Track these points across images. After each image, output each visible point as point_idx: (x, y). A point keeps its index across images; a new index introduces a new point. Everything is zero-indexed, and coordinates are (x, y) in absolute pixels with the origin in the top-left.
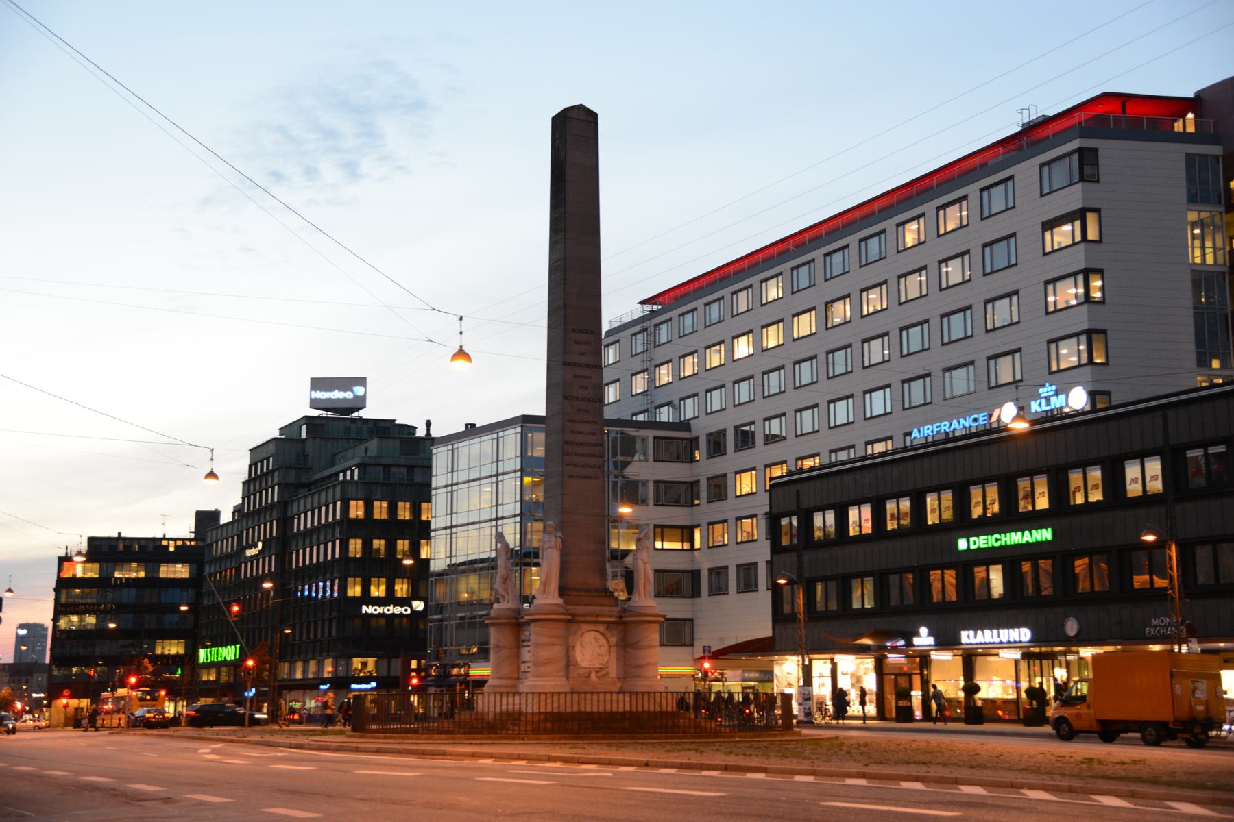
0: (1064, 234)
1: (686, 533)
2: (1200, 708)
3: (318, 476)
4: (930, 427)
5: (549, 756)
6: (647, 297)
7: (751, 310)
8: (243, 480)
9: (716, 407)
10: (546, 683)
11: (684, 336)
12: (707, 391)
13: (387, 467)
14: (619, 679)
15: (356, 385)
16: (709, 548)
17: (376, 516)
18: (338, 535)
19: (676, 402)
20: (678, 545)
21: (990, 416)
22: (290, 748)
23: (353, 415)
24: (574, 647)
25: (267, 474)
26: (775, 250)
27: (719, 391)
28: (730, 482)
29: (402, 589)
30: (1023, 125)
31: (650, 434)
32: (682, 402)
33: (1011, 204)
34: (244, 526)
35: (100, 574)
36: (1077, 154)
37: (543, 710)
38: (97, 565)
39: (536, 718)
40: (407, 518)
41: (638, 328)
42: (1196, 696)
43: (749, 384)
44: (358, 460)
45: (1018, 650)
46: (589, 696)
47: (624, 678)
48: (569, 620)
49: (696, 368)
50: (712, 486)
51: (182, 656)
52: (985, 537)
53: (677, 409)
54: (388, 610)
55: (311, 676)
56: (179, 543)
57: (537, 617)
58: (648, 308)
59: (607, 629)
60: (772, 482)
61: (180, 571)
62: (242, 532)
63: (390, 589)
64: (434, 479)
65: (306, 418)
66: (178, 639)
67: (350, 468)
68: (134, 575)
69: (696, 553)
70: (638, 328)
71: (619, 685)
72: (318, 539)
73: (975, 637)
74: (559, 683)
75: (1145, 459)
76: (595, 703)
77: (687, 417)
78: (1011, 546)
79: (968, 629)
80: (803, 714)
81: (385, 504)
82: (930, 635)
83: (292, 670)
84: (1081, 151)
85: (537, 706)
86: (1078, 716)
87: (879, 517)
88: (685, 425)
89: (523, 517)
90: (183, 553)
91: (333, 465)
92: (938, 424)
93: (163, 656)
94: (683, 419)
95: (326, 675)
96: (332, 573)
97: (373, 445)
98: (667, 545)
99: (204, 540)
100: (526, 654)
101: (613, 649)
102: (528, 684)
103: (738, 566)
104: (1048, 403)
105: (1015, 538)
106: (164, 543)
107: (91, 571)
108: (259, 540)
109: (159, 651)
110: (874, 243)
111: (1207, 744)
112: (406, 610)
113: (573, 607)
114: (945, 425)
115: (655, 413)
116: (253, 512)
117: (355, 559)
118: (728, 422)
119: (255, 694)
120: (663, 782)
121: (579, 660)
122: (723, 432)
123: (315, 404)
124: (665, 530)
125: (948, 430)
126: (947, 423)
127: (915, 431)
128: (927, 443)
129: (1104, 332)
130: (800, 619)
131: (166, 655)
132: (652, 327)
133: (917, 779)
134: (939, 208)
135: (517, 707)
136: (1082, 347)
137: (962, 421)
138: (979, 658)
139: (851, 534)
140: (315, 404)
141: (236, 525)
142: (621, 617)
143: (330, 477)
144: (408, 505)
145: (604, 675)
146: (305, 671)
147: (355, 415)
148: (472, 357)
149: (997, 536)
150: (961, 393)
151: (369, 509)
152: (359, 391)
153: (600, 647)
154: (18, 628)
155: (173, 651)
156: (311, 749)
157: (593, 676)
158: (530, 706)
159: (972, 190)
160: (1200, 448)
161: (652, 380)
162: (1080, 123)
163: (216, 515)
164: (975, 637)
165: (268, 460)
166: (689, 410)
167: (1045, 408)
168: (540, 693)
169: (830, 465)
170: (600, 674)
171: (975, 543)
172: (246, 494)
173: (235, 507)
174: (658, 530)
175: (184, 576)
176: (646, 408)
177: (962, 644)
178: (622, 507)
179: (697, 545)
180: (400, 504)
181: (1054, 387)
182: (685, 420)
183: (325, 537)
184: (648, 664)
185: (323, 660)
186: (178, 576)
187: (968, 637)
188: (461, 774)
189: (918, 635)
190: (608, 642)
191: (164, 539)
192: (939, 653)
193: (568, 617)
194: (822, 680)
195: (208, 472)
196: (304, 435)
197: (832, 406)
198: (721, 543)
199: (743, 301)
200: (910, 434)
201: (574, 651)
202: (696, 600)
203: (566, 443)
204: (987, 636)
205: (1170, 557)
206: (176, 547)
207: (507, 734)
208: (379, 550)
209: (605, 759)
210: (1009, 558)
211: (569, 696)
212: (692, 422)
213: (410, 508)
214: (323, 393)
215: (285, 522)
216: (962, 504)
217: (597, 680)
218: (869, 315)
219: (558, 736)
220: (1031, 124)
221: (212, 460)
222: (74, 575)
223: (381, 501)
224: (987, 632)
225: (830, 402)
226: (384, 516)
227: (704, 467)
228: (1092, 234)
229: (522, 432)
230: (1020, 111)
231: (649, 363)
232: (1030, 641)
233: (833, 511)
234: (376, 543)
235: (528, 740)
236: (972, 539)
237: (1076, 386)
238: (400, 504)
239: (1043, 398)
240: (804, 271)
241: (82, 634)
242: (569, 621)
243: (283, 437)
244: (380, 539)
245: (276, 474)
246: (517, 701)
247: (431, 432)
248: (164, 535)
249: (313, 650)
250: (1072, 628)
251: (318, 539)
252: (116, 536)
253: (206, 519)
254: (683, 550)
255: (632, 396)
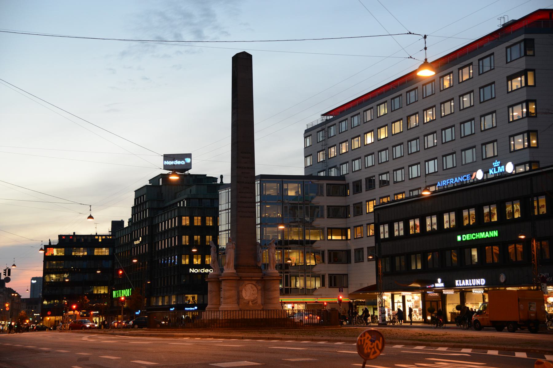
0: (516, 83)
1: (344, 232)
2: (533, 315)
3: (168, 204)
4: (445, 181)
5: (210, 336)
6: (324, 113)
7: (347, 130)
8: (132, 206)
9: (370, 164)
10: (228, 307)
11: (395, 110)
12: (393, 147)
13: (200, 200)
14: (262, 304)
15: (187, 157)
16: (355, 239)
17: (196, 224)
18: (177, 234)
19: (338, 166)
20: (339, 238)
21: (471, 176)
22: (120, 335)
23: (186, 172)
24: (242, 291)
25: (143, 203)
26: (384, 89)
27: (400, 146)
28: (364, 207)
29: (209, 260)
30: (503, 25)
31: (325, 183)
32: (341, 166)
33: (417, 100)
34: (133, 229)
35: (65, 253)
36: (523, 42)
37: (226, 318)
38: (63, 249)
39: (224, 321)
40: (211, 225)
41: (320, 129)
42: (531, 309)
43: (372, 156)
44: (186, 196)
45: (482, 289)
46: (246, 312)
47: (265, 304)
48: (239, 279)
49: (336, 154)
50: (356, 207)
51: (106, 294)
52: (469, 235)
53: (339, 169)
54: (202, 271)
55: (166, 304)
56: (104, 237)
57: (226, 278)
58: (325, 118)
59: (257, 283)
60: (375, 208)
61: (105, 252)
62: (132, 232)
63: (203, 260)
64: (220, 206)
65: (161, 174)
66: (104, 286)
67: (182, 200)
68: (81, 254)
69: (348, 241)
70: (320, 129)
71: (262, 307)
72: (168, 236)
73: (461, 283)
74: (234, 306)
75: (539, 197)
76: (248, 315)
77: (344, 174)
78: (480, 239)
79: (458, 280)
80: (381, 320)
81: (200, 218)
82: (442, 282)
83: (157, 302)
84: (525, 40)
85: (224, 316)
86: (483, 319)
87: (407, 228)
88: (343, 178)
89: (262, 225)
90: (106, 242)
91: (175, 198)
92: (449, 180)
93: (97, 295)
94: (341, 174)
95: (173, 303)
96: (174, 253)
97: (194, 188)
98: (334, 238)
99: (115, 236)
100: (222, 293)
101: (260, 292)
102: (223, 307)
103: (368, 248)
104: (497, 170)
105: (482, 235)
106: (97, 237)
107: (61, 252)
108: (140, 236)
109: (95, 292)
110: (487, 61)
111: (538, 332)
112: (211, 271)
113: (241, 274)
114: (452, 180)
115: (329, 171)
116: (137, 222)
117: (186, 245)
118: (363, 176)
119: (140, 313)
120: (234, 343)
121: (244, 296)
122: (361, 181)
123: (166, 167)
124: (333, 230)
125: (453, 183)
126: (453, 179)
127: (439, 183)
128: (444, 189)
129: (536, 131)
130: (379, 275)
131: (99, 294)
132: (327, 128)
133: (340, 341)
134: (459, 69)
135: (215, 317)
136: (512, 143)
137: (459, 178)
138: (467, 293)
139: (411, 233)
140: (166, 167)
141: (129, 229)
142: (262, 278)
143: (173, 204)
144: (211, 218)
145: (255, 303)
146: (163, 302)
147: (187, 172)
148: (94, 217)
149: (474, 234)
150: (469, 162)
151: (192, 221)
152: (188, 160)
153: (254, 290)
154: (31, 280)
155: (102, 292)
156: (127, 336)
157: (250, 303)
158: (221, 316)
159: (475, 60)
160: (495, 204)
161: (327, 155)
162: (525, 26)
163: (122, 222)
164: (461, 283)
165: (143, 196)
166: (344, 169)
167: (495, 172)
168: (225, 311)
169: (410, 198)
170: (253, 303)
171: (464, 237)
172: (133, 213)
173: (129, 219)
174: (329, 230)
175: (106, 254)
176: (324, 168)
177: (456, 286)
178: (280, 226)
179: (349, 237)
180: (207, 218)
181: (499, 162)
182: (343, 175)
183: (171, 235)
184: (274, 298)
185: (171, 296)
186: (104, 254)
187: (459, 283)
188: (166, 342)
189: (437, 282)
190: (257, 289)
191: (96, 235)
192: (447, 291)
193: (238, 278)
194: (399, 304)
195: (89, 216)
196: (161, 184)
197: (463, 153)
198: (360, 236)
199: (369, 116)
200: (488, 172)
201: (242, 293)
202: (349, 265)
203: (238, 202)
204: (466, 283)
205: (533, 246)
206: (102, 239)
207: (209, 328)
208: (197, 241)
209: (229, 336)
210: (480, 244)
211: (237, 312)
212: (345, 176)
213: (212, 219)
214: (170, 162)
215: (153, 227)
216: (459, 218)
217: (252, 305)
218: (427, 122)
219: (227, 329)
220: (509, 23)
221: (91, 210)
222: (53, 254)
223: (198, 216)
224: (467, 281)
225: (443, 156)
226: (199, 224)
227: (352, 199)
228: (531, 82)
229: (260, 183)
230: (500, 19)
231: (325, 146)
232: (484, 285)
233: (454, 212)
234: (196, 237)
235: (214, 330)
236: (463, 236)
237: (507, 163)
238: (207, 218)
239: (495, 167)
240: (397, 100)
241: (56, 284)
242: (239, 280)
243: (151, 184)
244: (198, 235)
245: (147, 203)
246: (215, 314)
247: (223, 181)
248: (96, 233)
249: (167, 291)
250: (502, 278)
251: (168, 236)
252: (73, 234)
253: (117, 225)
254: (342, 240)
255: (318, 163)
